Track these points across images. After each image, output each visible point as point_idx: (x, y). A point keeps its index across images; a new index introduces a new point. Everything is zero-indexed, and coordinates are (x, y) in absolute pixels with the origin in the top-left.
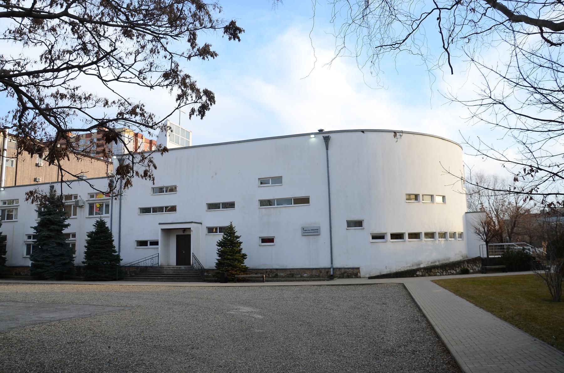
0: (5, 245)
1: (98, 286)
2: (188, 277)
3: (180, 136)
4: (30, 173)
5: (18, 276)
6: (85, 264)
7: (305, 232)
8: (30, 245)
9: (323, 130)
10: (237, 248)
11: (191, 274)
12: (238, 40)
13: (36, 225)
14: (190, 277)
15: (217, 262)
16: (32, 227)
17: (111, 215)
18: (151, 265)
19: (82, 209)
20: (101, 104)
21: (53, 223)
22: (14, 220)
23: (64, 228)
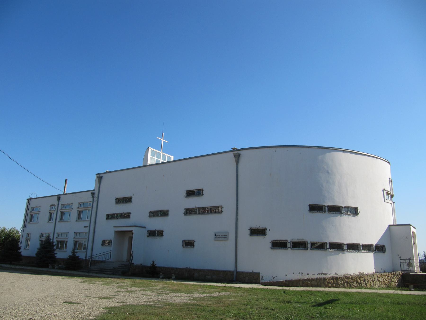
3: (163, 140)
7: (216, 237)
18: (105, 260)
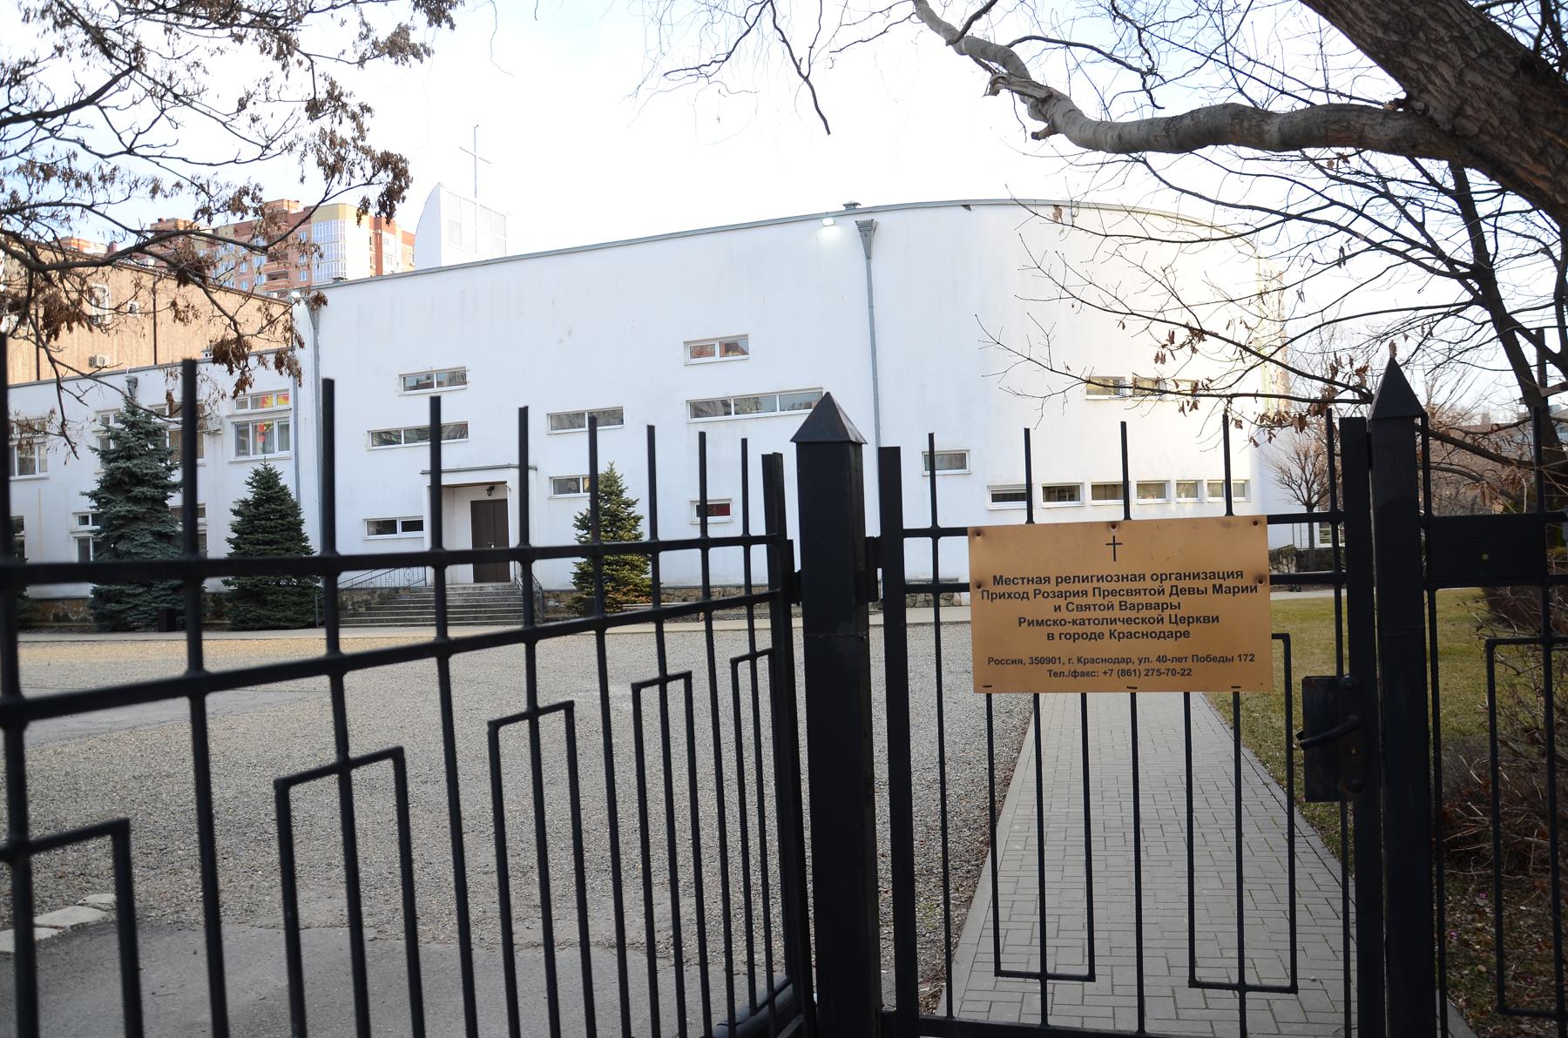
0: (22, 544)
1: (263, 642)
2: (502, 612)
4: (76, 345)
5: (62, 624)
6: (232, 587)
8: (87, 540)
9: (857, 204)
10: (629, 531)
11: (509, 606)
12: (448, 25)
13: (96, 487)
14: (510, 611)
15: (576, 570)
16: (83, 494)
17: (296, 454)
18: (407, 584)
19: (218, 439)
20: (144, 191)
21: (139, 480)
22: (38, 474)
23: (169, 494)
